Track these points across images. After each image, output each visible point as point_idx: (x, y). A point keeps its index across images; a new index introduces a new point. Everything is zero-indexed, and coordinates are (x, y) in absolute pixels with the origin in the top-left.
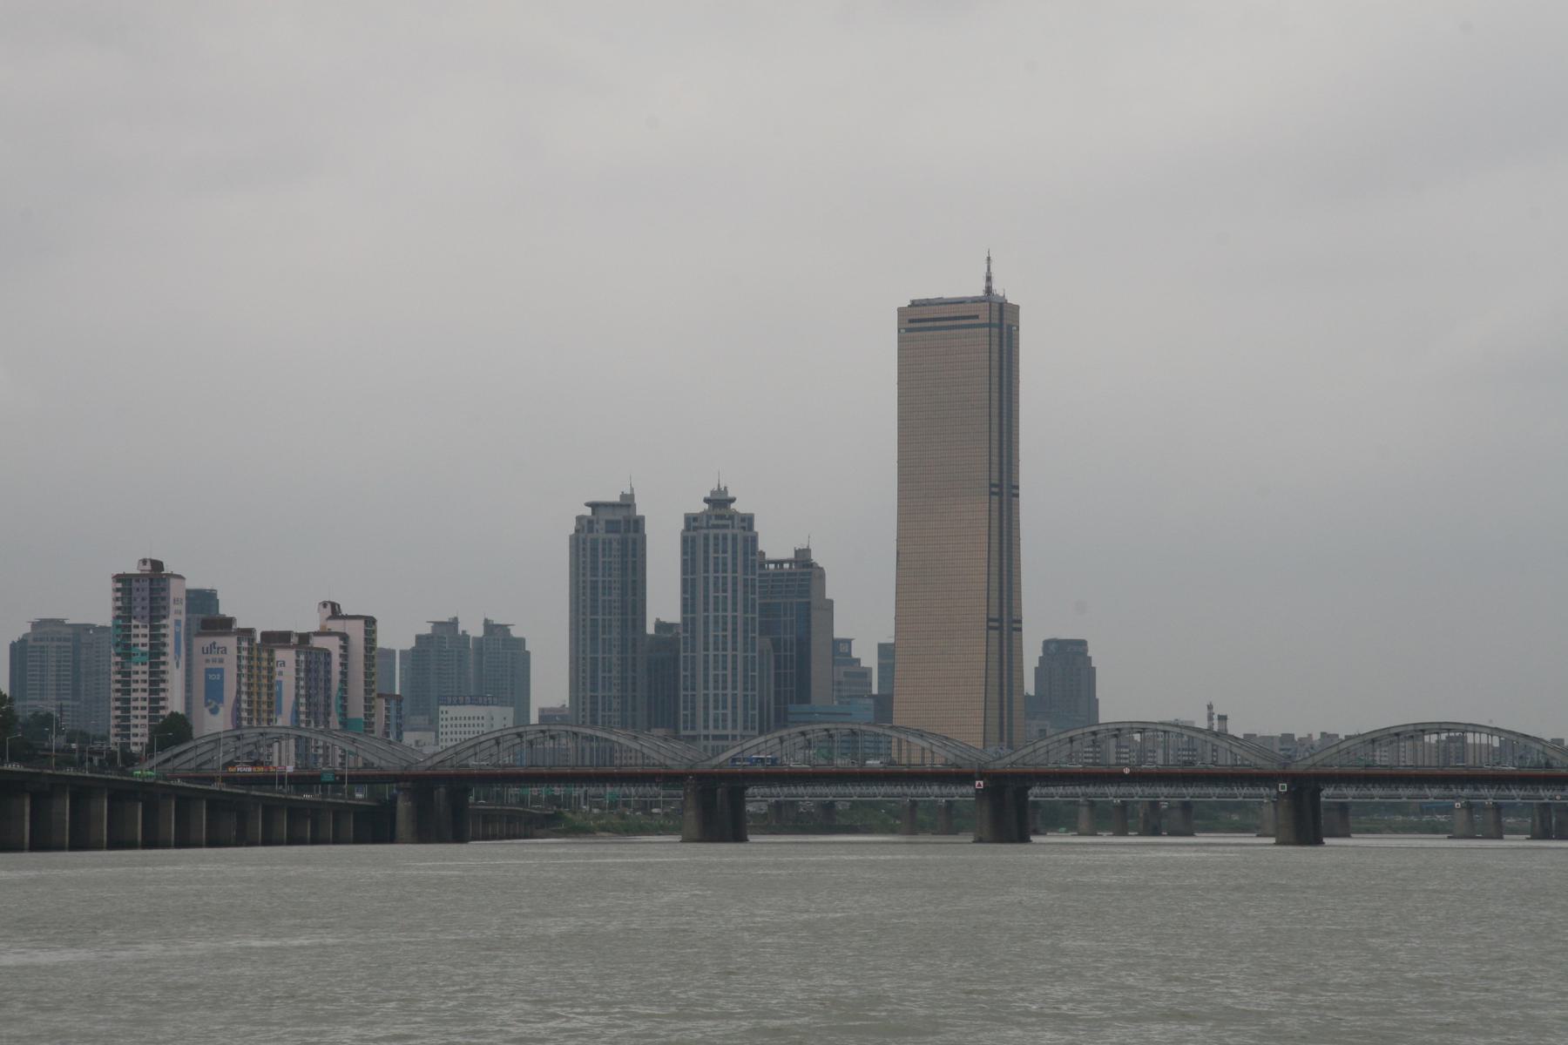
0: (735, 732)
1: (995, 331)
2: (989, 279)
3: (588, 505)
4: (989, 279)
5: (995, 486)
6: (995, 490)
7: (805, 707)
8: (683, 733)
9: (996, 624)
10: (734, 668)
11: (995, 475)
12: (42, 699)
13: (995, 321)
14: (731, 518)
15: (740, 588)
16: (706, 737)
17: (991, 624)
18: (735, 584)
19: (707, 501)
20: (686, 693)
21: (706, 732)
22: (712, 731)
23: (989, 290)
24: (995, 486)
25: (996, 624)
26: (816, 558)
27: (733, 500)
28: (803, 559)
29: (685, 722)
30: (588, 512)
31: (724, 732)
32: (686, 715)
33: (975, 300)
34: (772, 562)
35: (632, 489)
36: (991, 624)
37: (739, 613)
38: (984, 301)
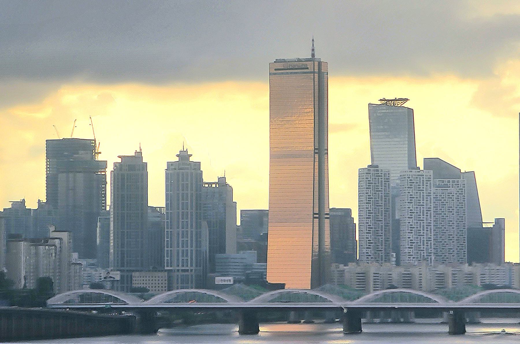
0: (192, 268)
1: (316, 75)
2: (313, 50)
3: (119, 157)
4: (313, 50)
5: (316, 149)
6: (316, 151)
7: (224, 255)
8: (166, 268)
9: (317, 216)
10: (192, 237)
11: (317, 145)
12: (188, 170)
13: (316, 70)
14: (190, 164)
15: (194, 216)
16: (178, 270)
17: (315, 216)
18: (192, 234)
19: (178, 156)
20: (168, 249)
21: (177, 268)
22: (180, 268)
23: (313, 55)
24: (316, 149)
25: (317, 216)
26: (228, 181)
27: (191, 155)
28: (222, 182)
29: (167, 263)
30: (119, 160)
31: (187, 268)
32: (168, 260)
33: (308, 60)
34: (207, 183)
35: (141, 150)
36: (315, 216)
37: (194, 230)
38: (311, 61)
